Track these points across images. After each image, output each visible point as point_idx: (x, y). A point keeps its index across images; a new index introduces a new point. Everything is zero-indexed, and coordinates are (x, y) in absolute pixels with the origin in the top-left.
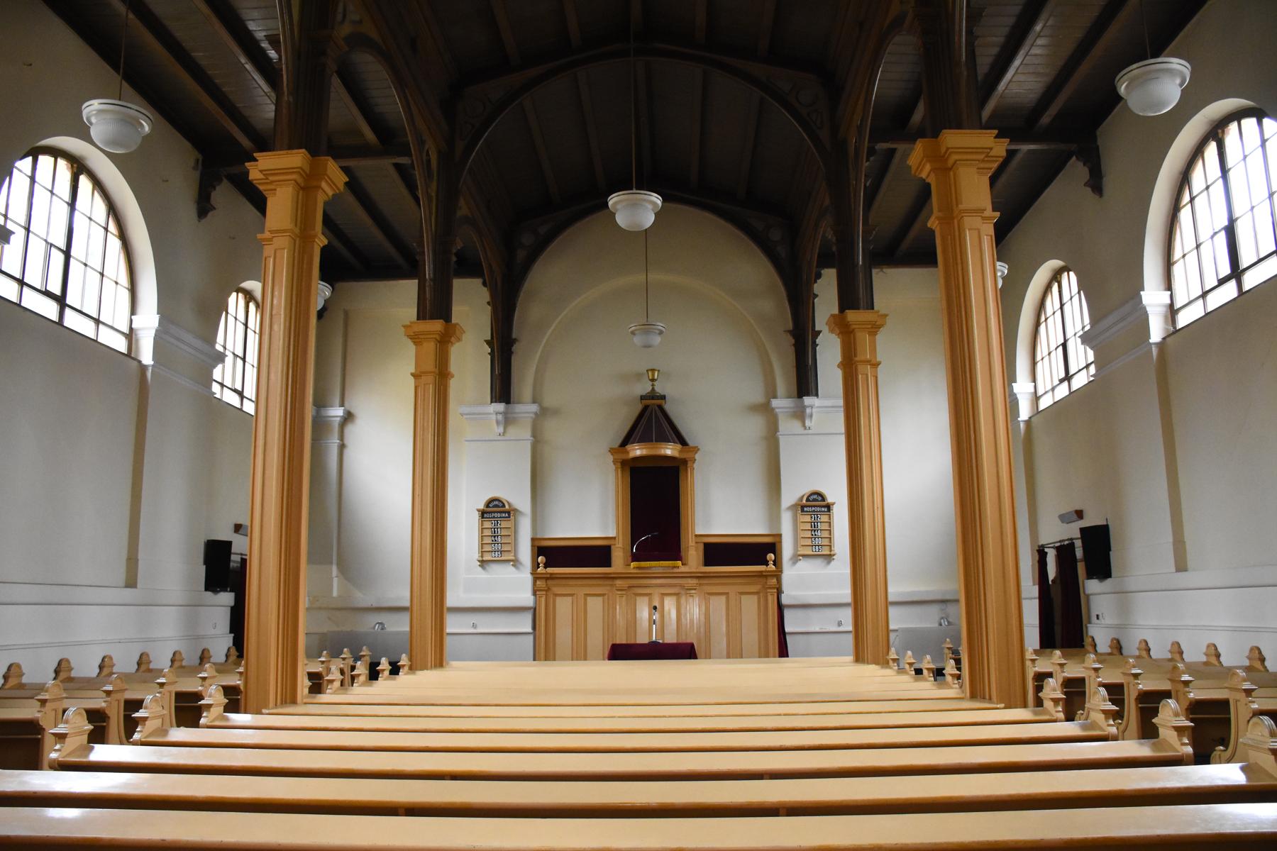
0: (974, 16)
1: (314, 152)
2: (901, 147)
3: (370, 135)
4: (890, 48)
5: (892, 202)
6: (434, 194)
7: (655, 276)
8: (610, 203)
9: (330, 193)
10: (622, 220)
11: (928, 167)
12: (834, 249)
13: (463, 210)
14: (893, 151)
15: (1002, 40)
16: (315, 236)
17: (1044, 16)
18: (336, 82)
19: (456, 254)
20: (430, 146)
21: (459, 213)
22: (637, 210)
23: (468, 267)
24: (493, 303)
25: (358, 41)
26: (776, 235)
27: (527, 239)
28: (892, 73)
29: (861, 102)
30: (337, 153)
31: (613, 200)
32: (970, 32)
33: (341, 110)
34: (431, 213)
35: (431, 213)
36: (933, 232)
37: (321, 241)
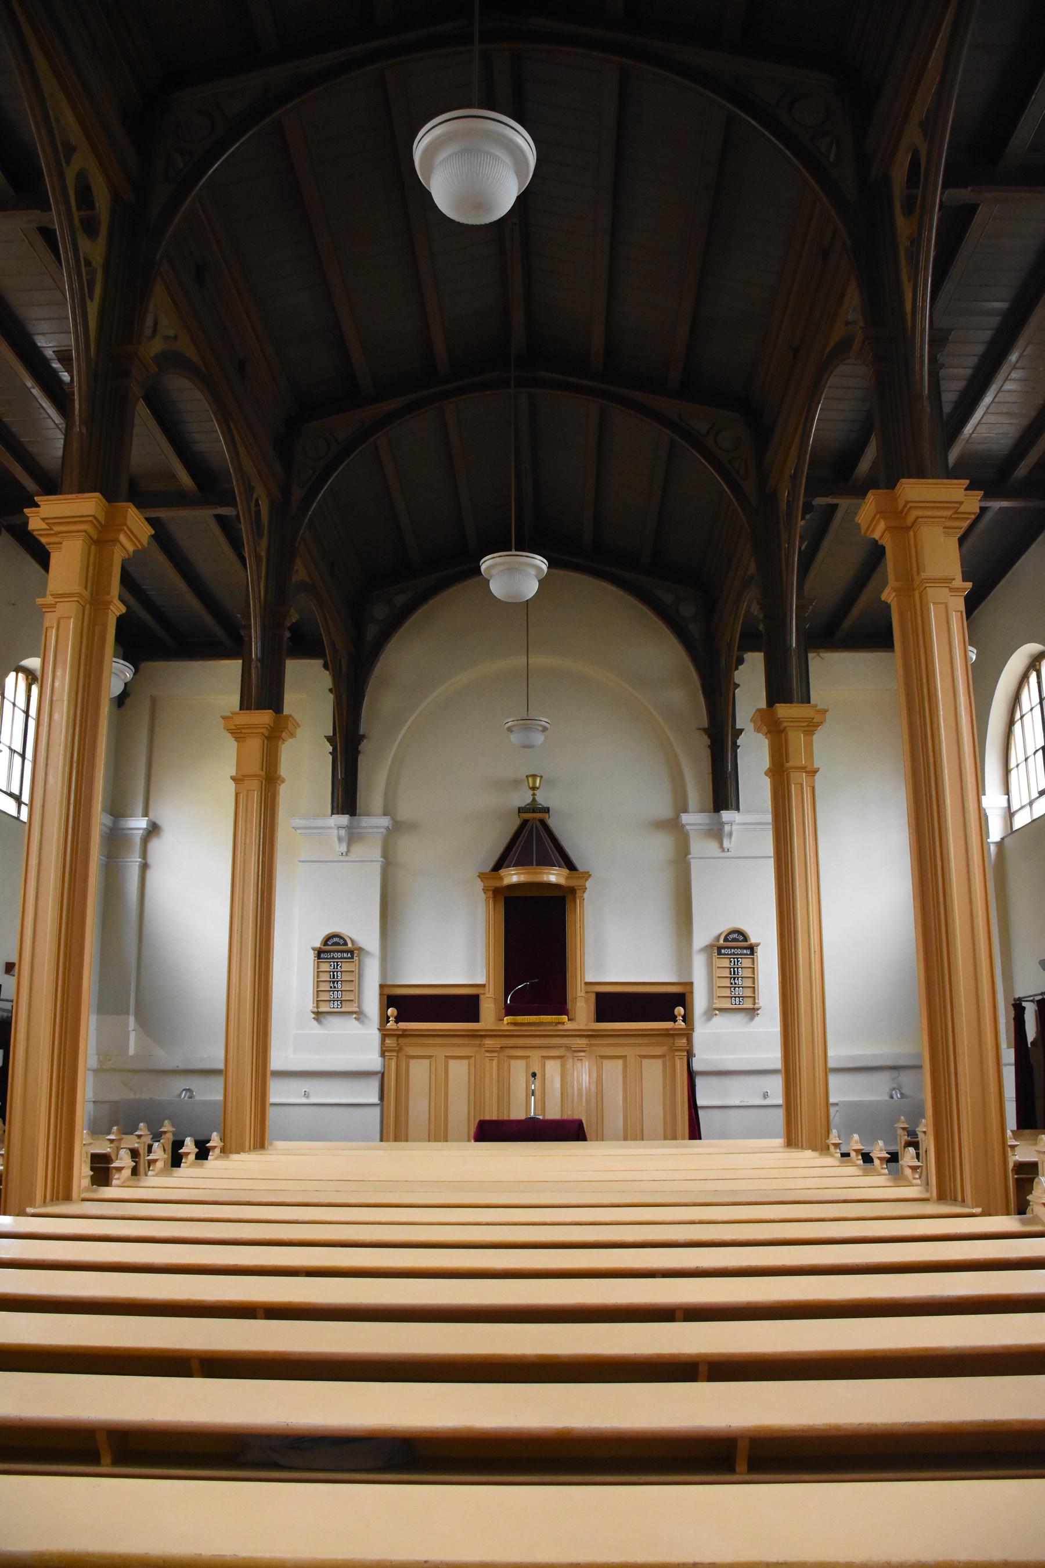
0: (939, 339)
1: (111, 497)
2: (844, 503)
3: (186, 480)
4: (832, 381)
5: (834, 569)
6: (263, 554)
7: (538, 660)
8: (483, 568)
9: (131, 548)
10: (497, 588)
11: (882, 525)
12: (761, 627)
13: (300, 573)
14: (835, 507)
15: (968, 372)
16: (110, 602)
17: (1021, 343)
18: (142, 412)
20: (260, 492)
21: (295, 578)
22: (516, 576)
23: (305, 645)
25: (172, 360)
26: (687, 610)
27: (380, 612)
30: (141, 499)
31: (487, 563)
32: (933, 360)
33: (147, 446)
37: (118, 609)
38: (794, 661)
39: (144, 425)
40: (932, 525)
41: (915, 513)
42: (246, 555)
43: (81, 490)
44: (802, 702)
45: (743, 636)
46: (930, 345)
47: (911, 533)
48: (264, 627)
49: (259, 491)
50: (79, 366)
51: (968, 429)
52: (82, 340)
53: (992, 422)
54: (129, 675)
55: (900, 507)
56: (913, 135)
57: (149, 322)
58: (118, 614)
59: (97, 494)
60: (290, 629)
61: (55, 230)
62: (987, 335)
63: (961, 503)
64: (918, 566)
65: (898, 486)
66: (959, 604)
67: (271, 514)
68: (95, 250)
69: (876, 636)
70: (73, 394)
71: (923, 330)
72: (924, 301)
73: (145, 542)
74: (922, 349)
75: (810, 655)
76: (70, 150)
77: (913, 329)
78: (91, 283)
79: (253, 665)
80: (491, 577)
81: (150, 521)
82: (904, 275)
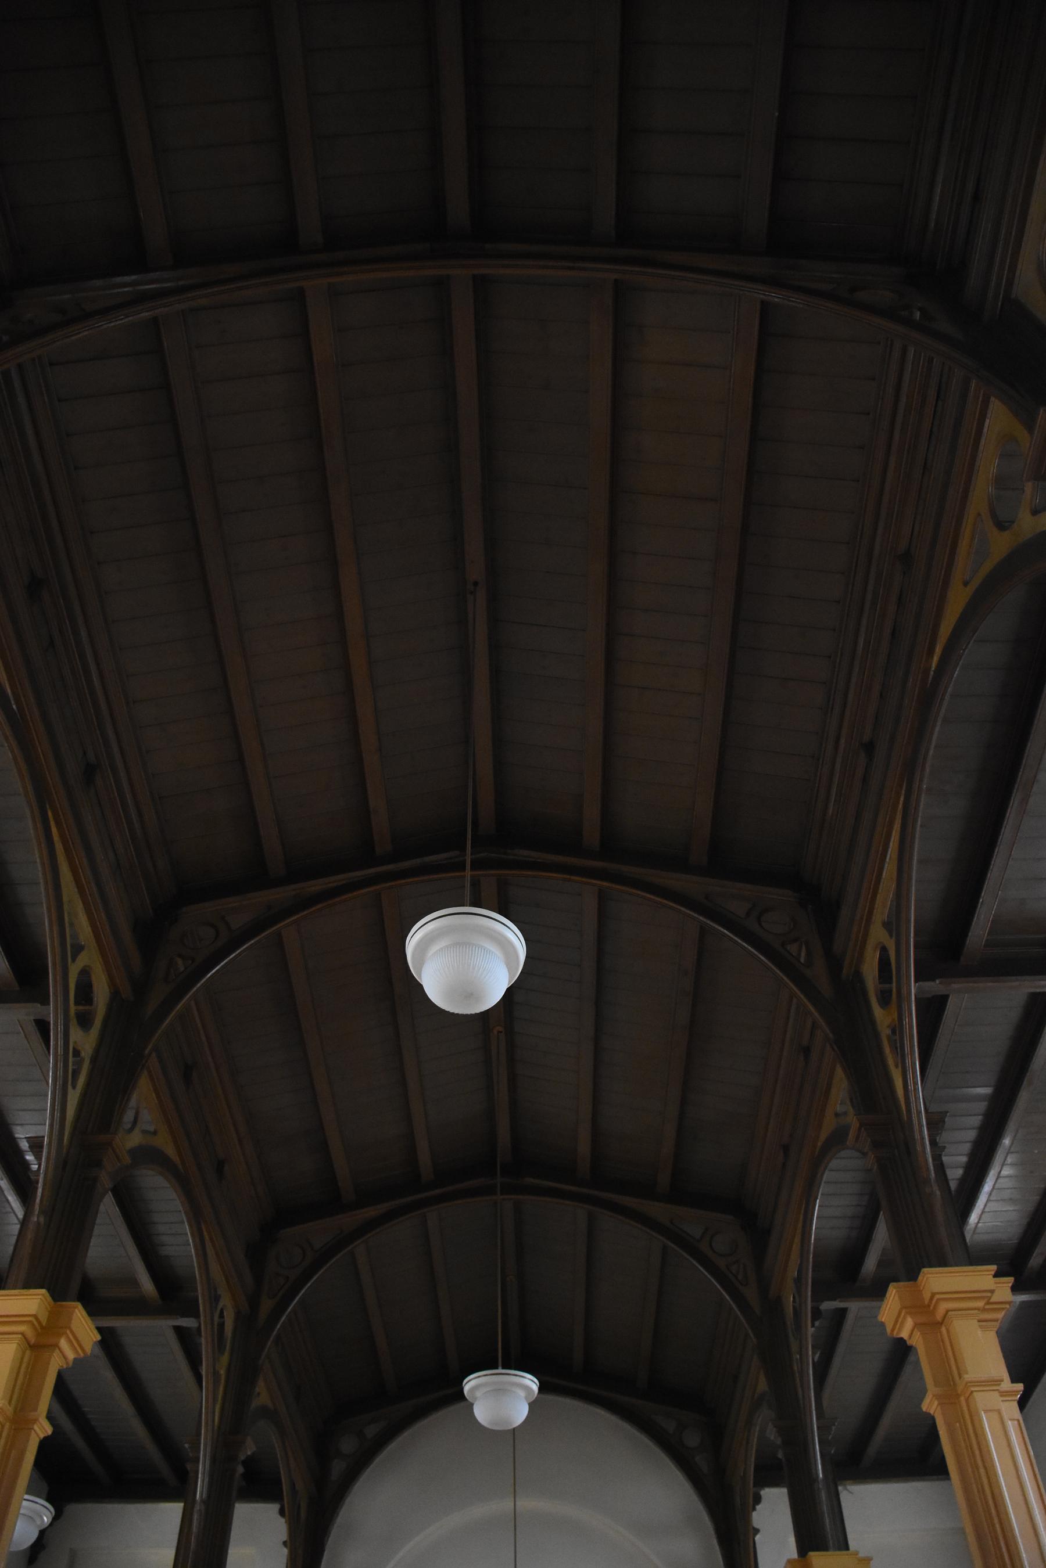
0: (936, 1123)
1: (58, 1294)
2: (854, 1307)
3: (147, 1285)
4: (827, 1176)
5: (853, 1378)
6: (222, 1372)
7: (527, 1504)
8: (467, 1389)
9: (71, 1356)
10: (482, 1413)
11: (909, 1323)
12: (780, 1455)
13: (262, 1395)
14: (842, 1313)
15: (964, 1159)
16: (35, 1421)
17: (1011, 1126)
18: (108, 1206)
19: (244, 1463)
20: (226, 1302)
21: (255, 1403)
22: (503, 1398)
23: (260, 1485)
24: (290, 1543)
25: (148, 1155)
26: (692, 1439)
27: (348, 1445)
28: (829, 1210)
29: (797, 1240)
30: (94, 1306)
31: (471, 1384)
32: (933, 1143)
33: (108, 1245)
34: (215, 1400)
35: (215, 1400)
36: (933, 1419)
37: (43, 1429)
38: (823, 1495)
39: (108, 1218)
40: (964, 1317)
41: (943, 1307)
42: (204, 1373)
43: (27, 1286)
44: (840, 1549)
45: (757, 1468)
46: (928, 1128)
47: (943, 1329)
48: (214, 1460)
49: (226, 1302)
50: (49, 1153)
51: (973, 1218)
52: (56, 1127)
53: (995, 1209)
54: (46, 1520)
55: (926, 1302)
56: (878, 934)
57: (129, 1116)
58: (42, 1436)
59: (44, 1291)
60: (244, 1463)
61: (49, 1023)
62: (976, 1121)
63: (992, 1291)
64: (958, 1368)
65: (920, 1278)
66: (1011, 1409)
67: (235, 1329)
68: (86, 1041)
69: (919, 1457)
70: (37, 1182)
71: (919, 1113)
72: (915, 1084)
73: (88, 1347)
74: (921, 1132)
75: (840, 1488)
76: (78, 949)
77: (909, 1110)
78: (76, 1073)
79: (197, 1507)
80: (476, 1399)
81: (99, 1329)
82: (890, 1062)
